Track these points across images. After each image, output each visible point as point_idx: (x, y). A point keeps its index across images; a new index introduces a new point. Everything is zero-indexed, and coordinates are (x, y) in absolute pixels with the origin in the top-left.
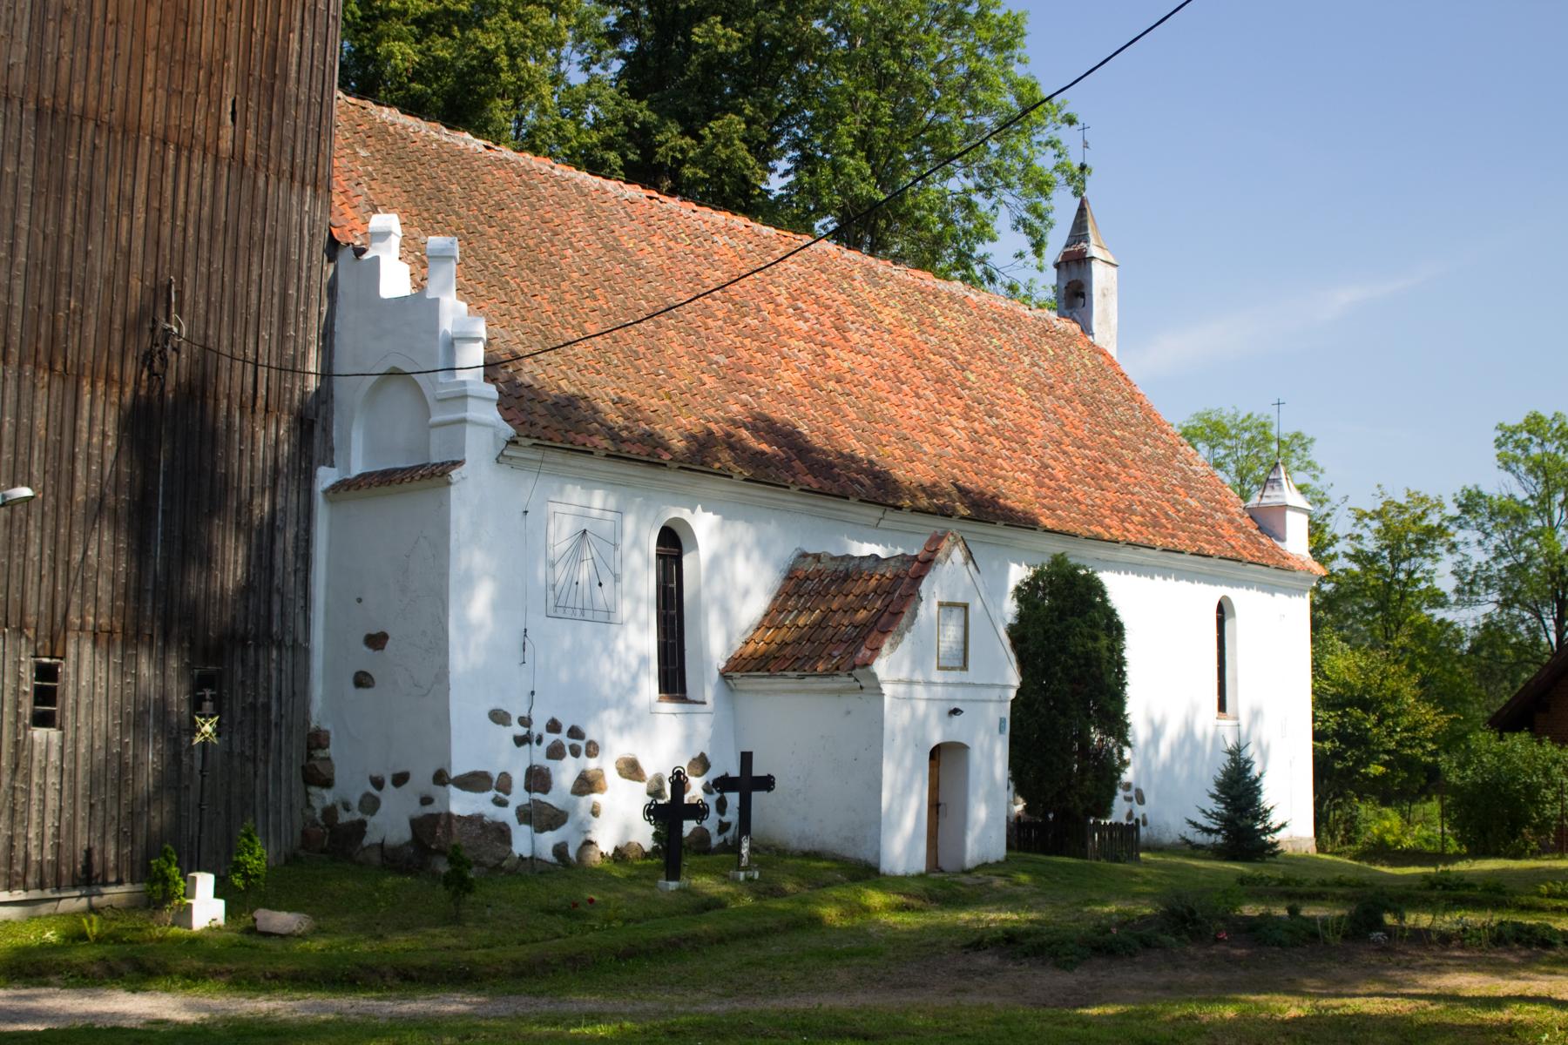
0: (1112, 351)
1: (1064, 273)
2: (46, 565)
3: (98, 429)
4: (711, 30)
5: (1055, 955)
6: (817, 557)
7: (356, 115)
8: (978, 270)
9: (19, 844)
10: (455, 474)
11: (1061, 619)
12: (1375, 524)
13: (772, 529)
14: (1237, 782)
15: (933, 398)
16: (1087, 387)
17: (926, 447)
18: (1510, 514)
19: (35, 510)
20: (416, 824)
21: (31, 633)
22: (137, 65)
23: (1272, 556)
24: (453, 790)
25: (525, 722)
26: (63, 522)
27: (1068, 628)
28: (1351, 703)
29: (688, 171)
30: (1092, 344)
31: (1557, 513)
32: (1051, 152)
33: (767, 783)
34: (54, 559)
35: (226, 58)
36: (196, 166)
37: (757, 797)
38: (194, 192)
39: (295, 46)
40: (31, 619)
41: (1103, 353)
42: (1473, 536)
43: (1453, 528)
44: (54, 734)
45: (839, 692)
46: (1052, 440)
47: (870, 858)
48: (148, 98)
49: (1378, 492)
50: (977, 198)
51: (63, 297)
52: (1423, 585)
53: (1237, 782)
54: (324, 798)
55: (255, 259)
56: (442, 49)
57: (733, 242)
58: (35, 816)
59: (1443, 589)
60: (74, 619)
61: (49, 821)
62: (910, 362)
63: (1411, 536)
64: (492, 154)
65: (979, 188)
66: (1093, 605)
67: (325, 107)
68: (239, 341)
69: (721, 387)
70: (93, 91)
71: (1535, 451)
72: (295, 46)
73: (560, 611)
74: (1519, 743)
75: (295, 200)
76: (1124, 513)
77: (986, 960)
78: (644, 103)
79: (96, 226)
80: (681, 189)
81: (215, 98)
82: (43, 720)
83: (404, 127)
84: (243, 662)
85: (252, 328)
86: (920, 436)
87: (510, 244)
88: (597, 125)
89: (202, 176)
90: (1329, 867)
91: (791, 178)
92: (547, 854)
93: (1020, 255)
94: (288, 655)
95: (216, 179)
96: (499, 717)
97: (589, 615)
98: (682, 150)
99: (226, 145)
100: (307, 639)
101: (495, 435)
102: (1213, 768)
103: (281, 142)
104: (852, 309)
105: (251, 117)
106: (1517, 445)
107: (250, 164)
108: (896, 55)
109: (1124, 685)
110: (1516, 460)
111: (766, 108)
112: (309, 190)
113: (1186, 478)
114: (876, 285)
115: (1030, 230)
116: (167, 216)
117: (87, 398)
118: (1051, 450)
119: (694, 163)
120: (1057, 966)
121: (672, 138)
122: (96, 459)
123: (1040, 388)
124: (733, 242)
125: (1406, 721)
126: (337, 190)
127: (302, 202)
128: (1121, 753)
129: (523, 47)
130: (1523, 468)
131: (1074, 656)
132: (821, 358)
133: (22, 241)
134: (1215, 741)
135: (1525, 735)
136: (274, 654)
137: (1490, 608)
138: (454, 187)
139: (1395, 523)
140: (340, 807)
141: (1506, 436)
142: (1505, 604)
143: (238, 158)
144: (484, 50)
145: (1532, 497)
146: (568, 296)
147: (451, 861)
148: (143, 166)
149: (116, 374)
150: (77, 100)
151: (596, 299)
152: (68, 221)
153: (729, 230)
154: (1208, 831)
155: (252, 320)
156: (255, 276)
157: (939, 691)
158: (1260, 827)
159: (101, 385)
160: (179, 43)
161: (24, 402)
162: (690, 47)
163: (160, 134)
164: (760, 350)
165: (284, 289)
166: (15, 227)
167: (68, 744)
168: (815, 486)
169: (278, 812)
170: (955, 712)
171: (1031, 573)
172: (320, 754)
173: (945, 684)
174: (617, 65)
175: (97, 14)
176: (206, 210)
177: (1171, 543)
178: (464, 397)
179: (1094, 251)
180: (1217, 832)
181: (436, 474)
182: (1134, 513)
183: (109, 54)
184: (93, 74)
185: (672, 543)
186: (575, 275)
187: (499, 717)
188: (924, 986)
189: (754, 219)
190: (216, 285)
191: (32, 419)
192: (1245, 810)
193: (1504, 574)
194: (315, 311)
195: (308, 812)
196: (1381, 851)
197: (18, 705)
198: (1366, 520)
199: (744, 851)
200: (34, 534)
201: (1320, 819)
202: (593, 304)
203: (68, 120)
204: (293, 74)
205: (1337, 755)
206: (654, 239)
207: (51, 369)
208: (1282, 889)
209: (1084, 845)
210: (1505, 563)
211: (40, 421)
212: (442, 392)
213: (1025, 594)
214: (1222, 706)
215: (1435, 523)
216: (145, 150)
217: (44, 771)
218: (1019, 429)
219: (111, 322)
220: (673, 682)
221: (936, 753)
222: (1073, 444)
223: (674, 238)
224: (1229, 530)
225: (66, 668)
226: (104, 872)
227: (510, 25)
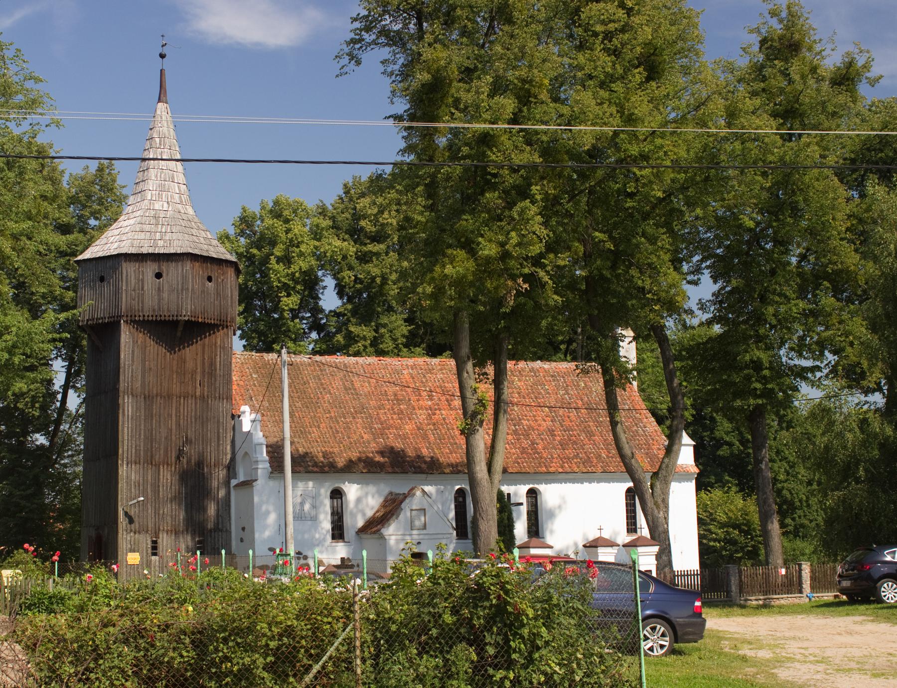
13: (382, 486)
44: (157, 558)
60: (161, 528)
82: (155, 554)
99: (198, 394)
157: (415, 537)
185: (337, 494)
200: (149, 507)
211: (149, 478)
225: (160, 541)
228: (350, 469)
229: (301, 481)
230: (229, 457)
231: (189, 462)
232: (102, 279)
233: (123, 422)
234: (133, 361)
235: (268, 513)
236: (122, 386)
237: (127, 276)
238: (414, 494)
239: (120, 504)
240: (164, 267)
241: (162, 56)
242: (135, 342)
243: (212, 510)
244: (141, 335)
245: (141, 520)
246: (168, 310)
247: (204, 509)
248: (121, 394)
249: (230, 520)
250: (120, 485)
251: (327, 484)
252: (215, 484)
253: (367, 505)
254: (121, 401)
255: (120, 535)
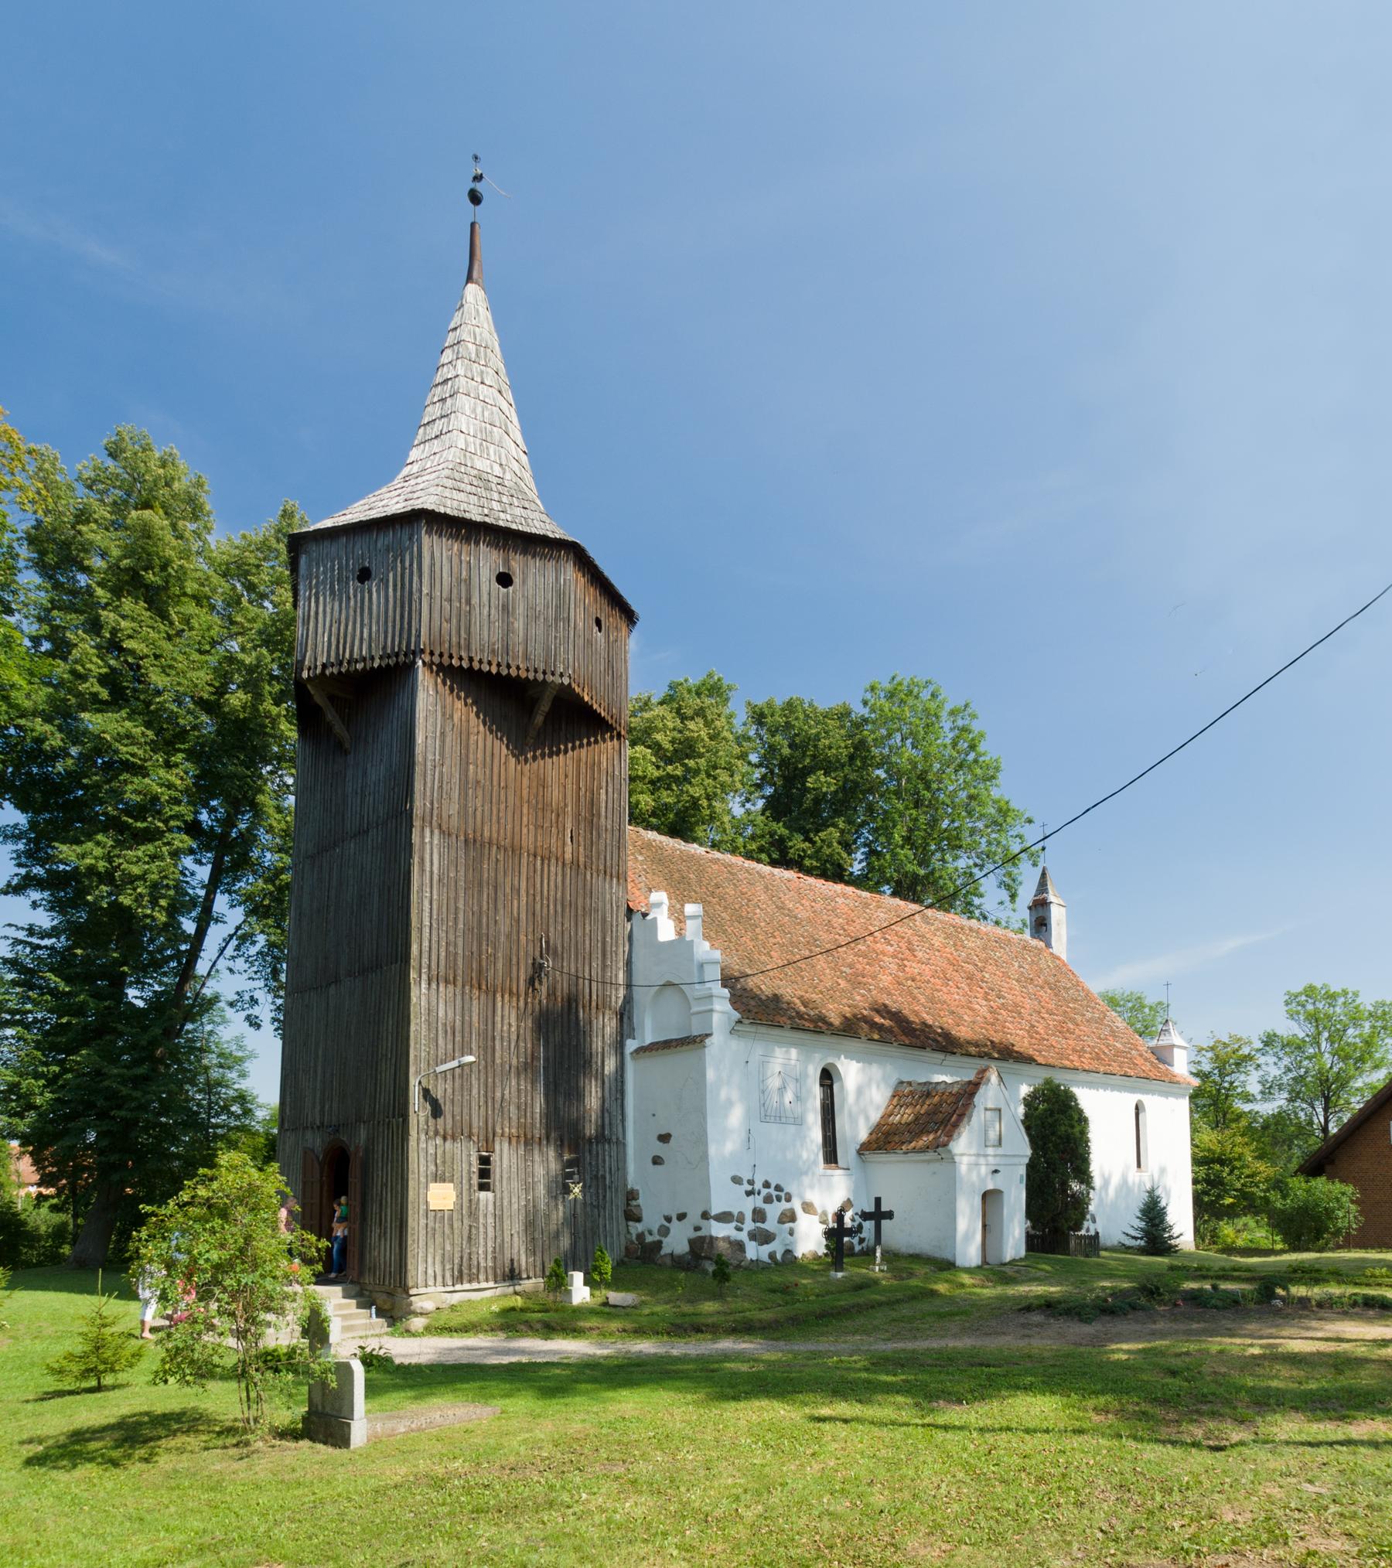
0: (1064, 957)
1: (1034, 912)
2: (482, 1099)
3: (506, 1021)
4: (818, 779)
5: (1079, 1314)
6: (910, 1084)
7: (634, 836)
8: (977, 913)
9: (475, 1257)
10: (707, 1041)
11: (1051, 1115)
12: (1210, 1055)
13: (889, 1068)
14: (1153, 1209)
15: (967, 989)
16: (1051, 980)
17: (966, 1017)
18: (1294, 1046)
19: (475, 1069)
20: (691, 1242)
21: (475, 1139)
22: (518, 812)
23: (1167, 1075)
24: (713, 1222)
25: (751, 1182)
26: (490, 1075)
27: (1056, 1121)
28: (1213, 1161)
29: (807, 862)
30: (1051, 954)
31: (1323, 1045)
32: (1018, 840)
33: (889, 1215)
34: (486, 1096)
35: (566, 805)
36: (553, 869)
37: (885, 1223)
38: (552, 884)
39: (603, 797)
40: (475, 1131)
41: (1058, 958)
42: (1271, 1059)
43: (1258, 1055)
44: (490, 1195)
45: (929, 1162)
46: (1035, 1011)
47: (950, 1257)
48: (525, 830)
49: (1211, 1035)
50: (975, 870)
51: (484, 947)
52: (1239, 1090)
53: (1153, 1209)
54: (636, 1228)
55: (587, 921)
56: (667, 797)
57: (847, 902)
58: (482, 1241)
59: (1252, 1092)
60: (499, 1131)
61: (490, 1244)
62: (951, 968)
63: (1232, 1061)
64: (709, 856)
65: (976, 865)
66: (1071, 1107)
67: (621, 831)
68: (580, 969)
69: (849, 986)
70: (494, 829)
71: (1310, 1007)
72: (603, 797)
73: (768, 1119)
74: (1320, 1184)
75: (607, 886)
76: (1080, 1052)
77: (1036, 1318)
78: (781, 824)
79: (500, 906)
80: (809, 872)
81: (561, 829)
82: (483, 1187)
83: (661, 842)
84: (590, 1151)
85: (587, 961)
86: (960, 1011)
87: (725, 908)
88: (753, 838)
89: (556, 874)
90: (1203, 1259)
91: (864, 864)
92: (765, 1258)
93: (1001, 903)
94: (614, 1147)
95: (564, 876)
96: (737, 1180)
97: (783, 1120)
98: (804, 850)
99: (568, 856)
100: (624, 1137)
101: (729, 1018)
102: (1139, 1200)
103: (598, 853)
104: (916, 938)
105: (581, 839)
106: (1299, 1004)
107: (582, 867)
108: (928, 788)
109: (1089, 1154)
110: (1298, 1013)
111: (850, 822)
112: (615, 880)
113: (1112, 1031)
114: (928, 923)
115: (1008, 887)
116: (538, 898)
117: (499, 1004)
118: (1035, 1017)
119: (810, 857)
120: (1081, 1321)
121: (798, 843)
122: (506, 1039)
123: (1025, 980)
124: (847, 902)
125: (1247, 1172)
126: (629, 880)
127: (611, 888)
128: (1088, 1193)
129: (715, 794)
130: (1302, 1018)
131: (1060, 1137)
132: (902, 967)
133: (461, 916)
134: (1140, 1185)
135: (1324, 1178)
136: (607, 1146)
137: (1283, 1103)
138: (691, 876)
139: (1222, 1053)
140: (646, 1233)
141: (1291, 999)
142: (1290, 1100)
143: (575, 863)
144: (692, 797)
145: (1308, 1035)
146: (760, 937)
147: (717, 1263)
148: (524, 870)
149: (515, 990)
150: (486, 834)
151: (775, 937)
152: (485, 903)
153: (844, 895)
154: (1135, 1238)
155: (587, 957)
156: (587, 931)
158: (1166, 1235)
159: (507, 996)
160: (540, 798)
161: (466, 1008)
162: (807, 790)
163: (532, 851)
164: (868, 964)
165: (604, 938)
166: (456, 908)
167: (498, 1201)
168: (907, 1042)
169: (612, 1237)
170: (996, 1171)
171: (1032, 1089)
172: (634, 1203)
173: (995, 1156)
174: (761, 803)
175: (495, 783)
176: (559, 894)
177: (1108, 1069)
178: (711, 996)
179: (1051, 898)
180: (1141, 1239)
181: (694, 1042)
182: (1085, 1052)
183: (503, 806)
184: (494, 818)
185: (827, 1077)
186: (763, 924)
187: (737, 1180)
188: (1004, 1333)
189: (858, 888)
190: (566, 937)
191: (471, 1017)
192: (1158, 1225)
193: (1291, 1082)
194: (621, 950)
195: (628, 1236)
196: (1229, 1250)
197: (470, 1179)
198: (1204, 1052)
199: (878, 1254)
200: (475, 1083)
201: (1196, 1230)
202: (774, 941)
203: (482, 845)
204: (603, 813)
205: (1205, 1193)
206: (804, 902)
207: (480, 988)
208: (1199, 1273)
209: (1068, 1248)
210: (1291, 1075)
211: (475, 1019)
212: (697, 994)
213: (1029, 1102)
214: (1139, 1165)
215: (1247, 1053)
216: (524, 861)
217: (486, 1216)
218: (1016, 1005)
219: (511, 960)
220: (831, 1156)
221: (986, 1196)
222: (1047, 1013)
223: (814, 901)
224: (1139, 1061)
225: (495, 1158)
226: (520, 1273)
227: (707, 781)
228: (850, 1029)
229: (780, 1044)
230: (622, 993)
231: (552, 993)
232: (364, 575)
233: (421, 890)
234: (442, 754)
235: (730, 1103)
236: (419, 805)
237: (432, 565)
238: (989, 1080)
239: (412, 1069)
240: (517, 564)
241: (475, 198)
242: (447, 717)
243: (593, 1100)
244: (459, 704)
245: (457, 1110)
246: (526, 657)
247: (578, 1095)
248: (417, 823)
249: (623, 1120)
250: (413, 1028)
251: (817, 1056)
252: (597, 1044)
253: (871, 1101)
254: (415, 838)
255: (412, 1143)
